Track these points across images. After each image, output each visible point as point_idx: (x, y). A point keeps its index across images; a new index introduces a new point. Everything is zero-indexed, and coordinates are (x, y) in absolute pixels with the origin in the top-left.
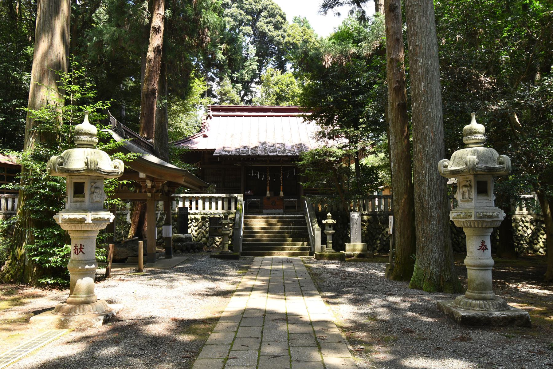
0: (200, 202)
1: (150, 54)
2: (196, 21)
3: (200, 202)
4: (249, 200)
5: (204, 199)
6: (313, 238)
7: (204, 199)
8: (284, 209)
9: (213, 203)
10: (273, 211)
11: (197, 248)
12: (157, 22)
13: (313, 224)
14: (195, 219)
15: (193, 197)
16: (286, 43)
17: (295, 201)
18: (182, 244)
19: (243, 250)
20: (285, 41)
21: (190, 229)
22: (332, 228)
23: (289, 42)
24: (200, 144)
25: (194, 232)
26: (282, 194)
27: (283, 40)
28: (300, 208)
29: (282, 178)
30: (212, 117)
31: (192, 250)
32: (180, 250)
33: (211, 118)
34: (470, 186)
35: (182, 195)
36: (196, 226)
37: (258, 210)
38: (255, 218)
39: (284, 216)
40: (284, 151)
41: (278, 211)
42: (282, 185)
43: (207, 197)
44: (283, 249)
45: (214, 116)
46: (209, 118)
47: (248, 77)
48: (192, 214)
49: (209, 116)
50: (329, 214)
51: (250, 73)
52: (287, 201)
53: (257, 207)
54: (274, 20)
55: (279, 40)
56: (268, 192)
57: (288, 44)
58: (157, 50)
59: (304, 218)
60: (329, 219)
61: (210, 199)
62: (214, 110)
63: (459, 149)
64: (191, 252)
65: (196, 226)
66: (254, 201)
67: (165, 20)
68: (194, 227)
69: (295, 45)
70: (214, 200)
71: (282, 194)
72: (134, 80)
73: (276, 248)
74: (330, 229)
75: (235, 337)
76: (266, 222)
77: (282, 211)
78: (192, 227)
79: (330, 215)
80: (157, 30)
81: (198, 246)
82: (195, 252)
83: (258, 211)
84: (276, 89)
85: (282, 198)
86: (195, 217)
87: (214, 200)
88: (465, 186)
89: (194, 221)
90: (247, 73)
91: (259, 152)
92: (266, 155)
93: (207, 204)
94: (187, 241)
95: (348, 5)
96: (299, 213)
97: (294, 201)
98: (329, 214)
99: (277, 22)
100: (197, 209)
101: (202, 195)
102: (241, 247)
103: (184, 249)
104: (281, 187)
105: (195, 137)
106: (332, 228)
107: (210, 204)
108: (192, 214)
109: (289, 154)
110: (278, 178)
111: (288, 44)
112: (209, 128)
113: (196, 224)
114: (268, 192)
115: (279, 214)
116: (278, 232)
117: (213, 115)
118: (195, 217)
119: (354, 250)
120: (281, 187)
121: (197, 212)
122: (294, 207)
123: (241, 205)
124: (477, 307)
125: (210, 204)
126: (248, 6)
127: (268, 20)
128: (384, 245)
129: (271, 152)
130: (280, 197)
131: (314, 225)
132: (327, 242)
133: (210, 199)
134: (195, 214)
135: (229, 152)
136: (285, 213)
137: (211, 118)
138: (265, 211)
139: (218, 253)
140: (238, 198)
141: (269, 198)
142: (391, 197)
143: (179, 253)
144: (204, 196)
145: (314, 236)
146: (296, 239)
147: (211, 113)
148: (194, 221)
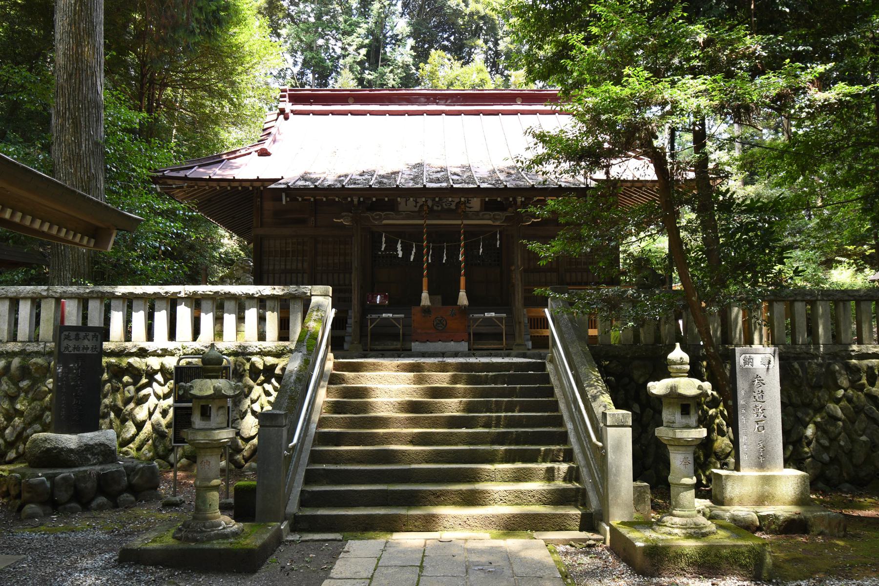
0: (184, 313)
3: (184, 313)
4: (374, 316)
5: (196, 302)
6: (600, 456)
7: (196, 302)
8: (469, 341)
9: (226, 316)
10: (439, 346)
11: (131, 489)
13: (591, 392)
14: (163, 370)
15: (157, 296)
16: (471, 15)
17: (500, 319)
18: (50, 478)
19: (307, 500)
20: (468, 11)
21: (145, 406)
22: (693, 419)
23: (478, 12)
25: (157, 416)
26: (463, 298)
27: (464, 8)
29: (465, 253)
30: (291, 115)
31: (102, 500)
32: (42, 503)
33: (286, 118)
35: (121, 290)
36: (166, 396)
37: (398, 345)
38: (375, 368)
39: (472, 360)
40: (471, 179)
41: (452, 346)
42: (465, 275)
43: (205, 297)
44: (472, 499)
45: (295, 112)
46: (282, 117)
47: (394, 80)
48: (154, 354)
49: (282, 111)
50: (678, 354)
51: (399, 71)
52: (478, 319)
53: (395, 337)
55: (458, 5)
56: (425, 295)
57: (476, 17)
59: (542, 367)
60: (679, 374)
61: (219, 304)
62: (295, 99)
64: (101, 508)
65: (166, 396)
66: (388, 318)
68: (158, 397)
69: (490, 19)
70: (228, 305)
71: (463, 298)
73: (443, 493)
74: (685, 421)
75: (377, 566)
76: (419, 380)
77: (464, 346)
78: (152, 401)
79: (686, 358)
81: (136, 480)
82: (116, 506)
83: (399, 346)
85: (464, 311)
86: (162, 366)
87: (228, 305)
89: (159, 377)
90: (391, 72)
92: (419, 186)
93: (207, 320)
94: (85, 462)
95: (382, 548)
96: (513, 352)
97: (496, 318)
98: (678, 354)
100: (172, 336)
101: (190, 289)
102: (298, 486)
103: (63, 495)
104: (463, 280)
105: (238, 154)
106: (693, 419)
107: (219, 320)
108: (154, 354)
109: (483, 186)
110: (452, 255)
111: (476, 17)
112: (278, 137)
113: (166, 389)
114: (425, 295)
115: (456, 355)
116: (453, 422)
117: (292, 111)
118: (162, 366)
119: (762, 500)
120: (463, 280)
121: (171, 346)
122: (497, 336)
123: (322, 321)
125: (219, 320)
128: (824, 464)
129: (431, 181)
130: (460, 307)
131: (595, 398)
132: (671, 478)
134: (165, 353)
135: (314, 181)
136: (471, 352)
137: (286, 118)
138: (416, 346)
139: (169, 540)
140: (314, 300)
141: (427, 310)
142: (836, 302)
143: (32, 517)
144: (195, 293)
145: (604, 448)
147: (288, 107)
148: (159, 377)
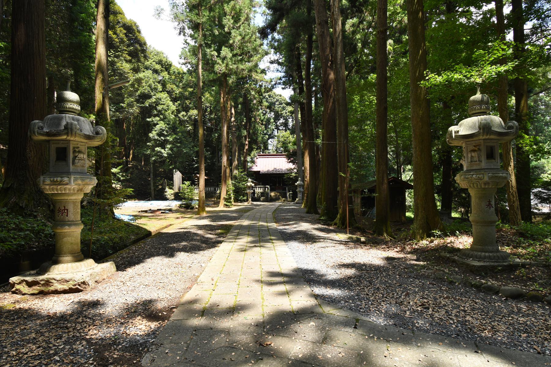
1: (245, 151)
2: (257, 141)
5: (259, 187)
7: (259, 187)
12: (247, 143)
24: (255, 169)
28: (285, 189)
34: (479, 149)
54: (282, 106)
58: (247, 150)
61: (260, 187)
63: (464, 119)
67: (249, 142)
72: (391, 339)
80: (247, 145)
84: (282, 139)
88: (474, 151)
91: (275, 172)
99: (283, 107)
124: (234, 185)
126: (270, 101)
127: (279, 106)
133: (260, 187)
146: (283, 197)
